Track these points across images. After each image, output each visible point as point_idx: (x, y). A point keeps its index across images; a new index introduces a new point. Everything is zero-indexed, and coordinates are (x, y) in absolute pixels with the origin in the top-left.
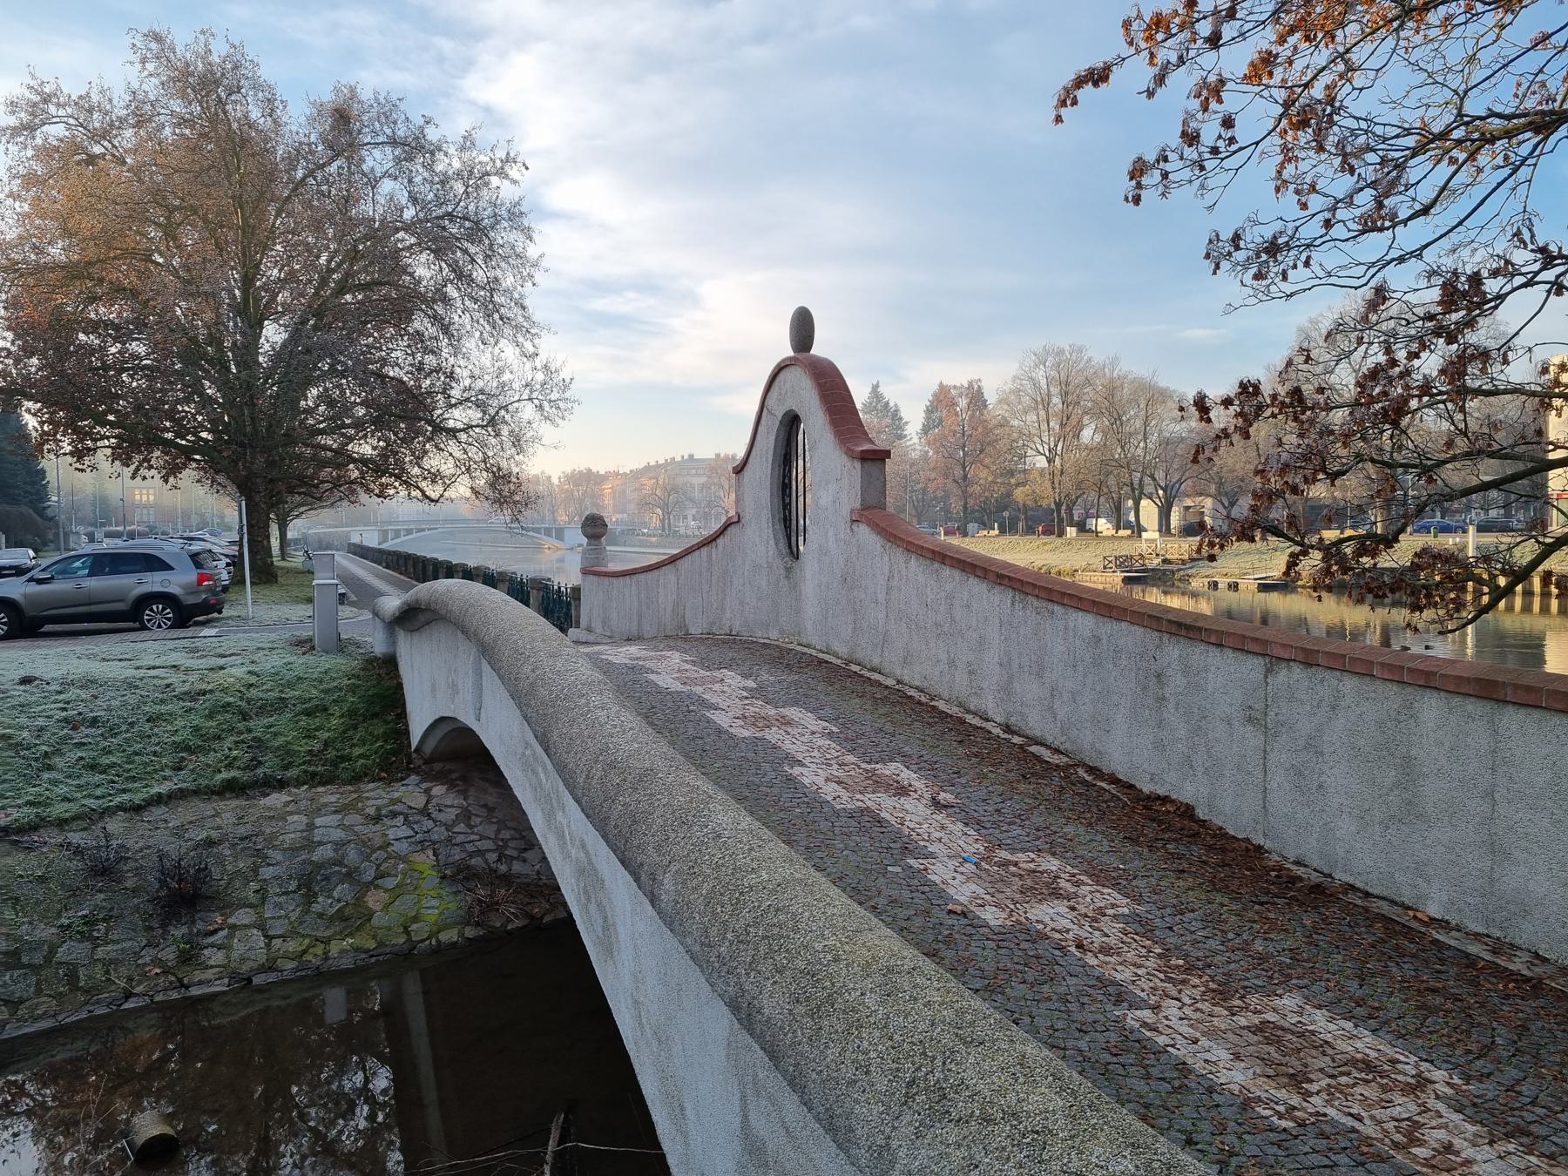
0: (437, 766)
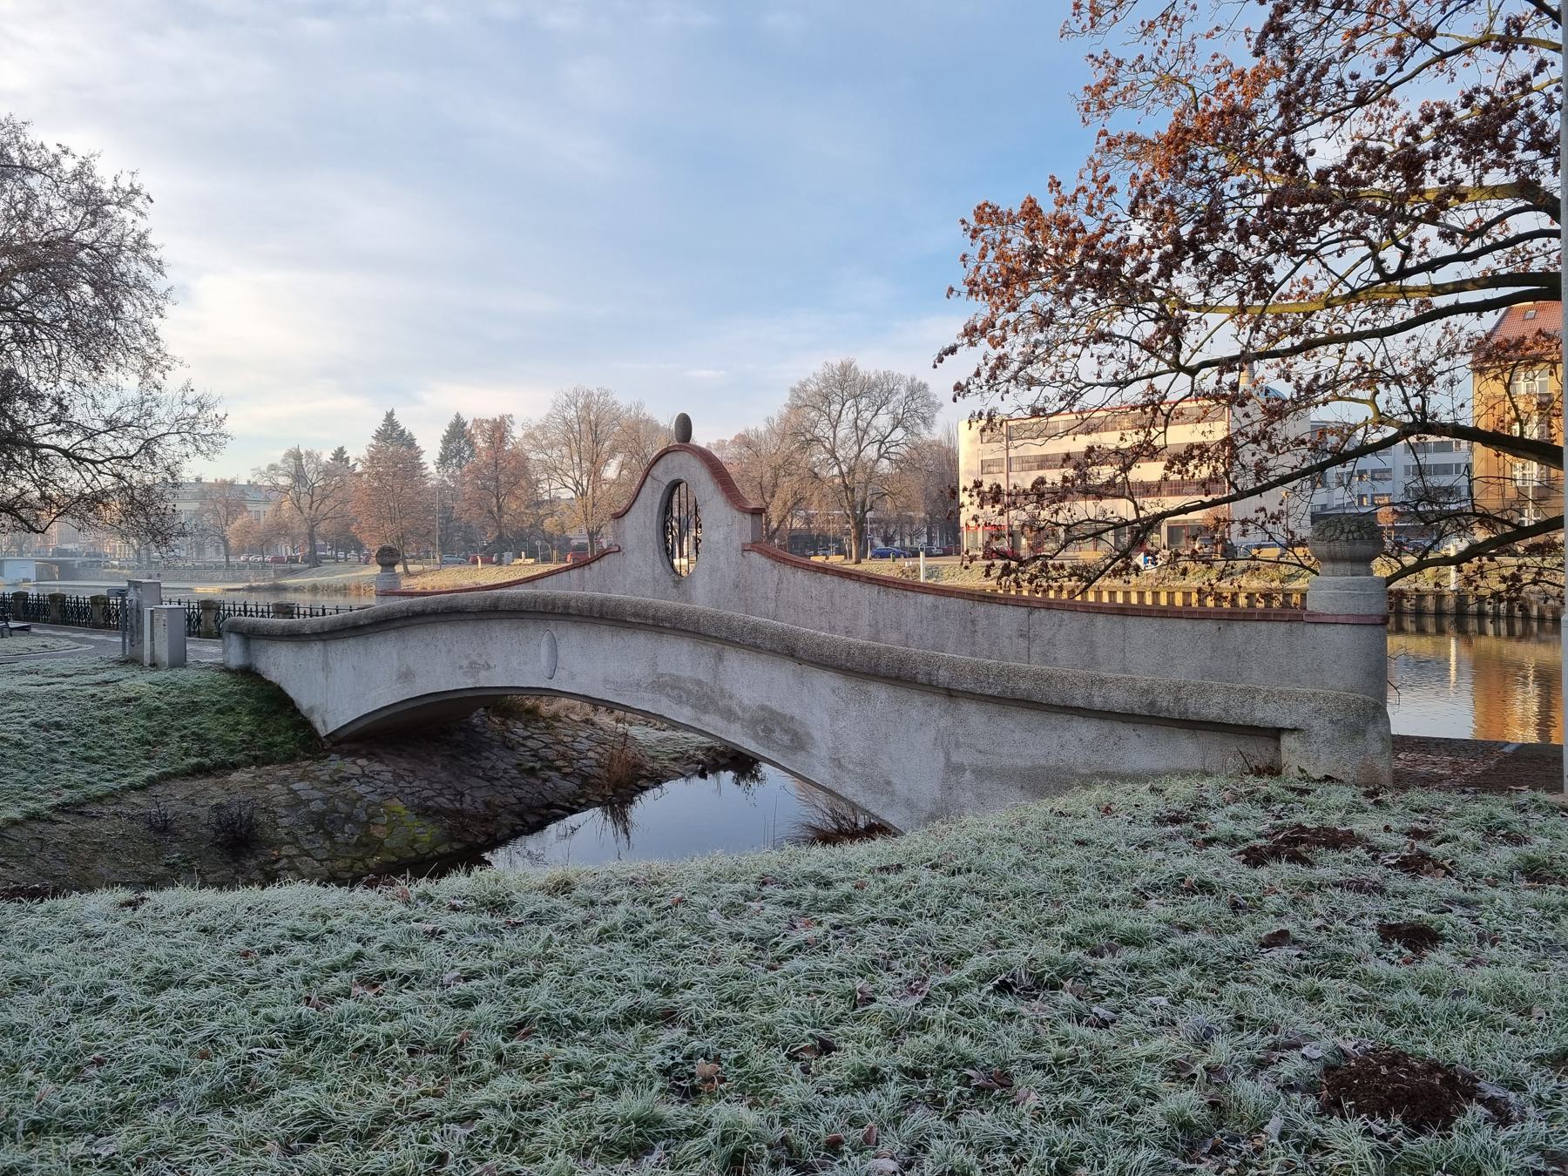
0: (345, 747)
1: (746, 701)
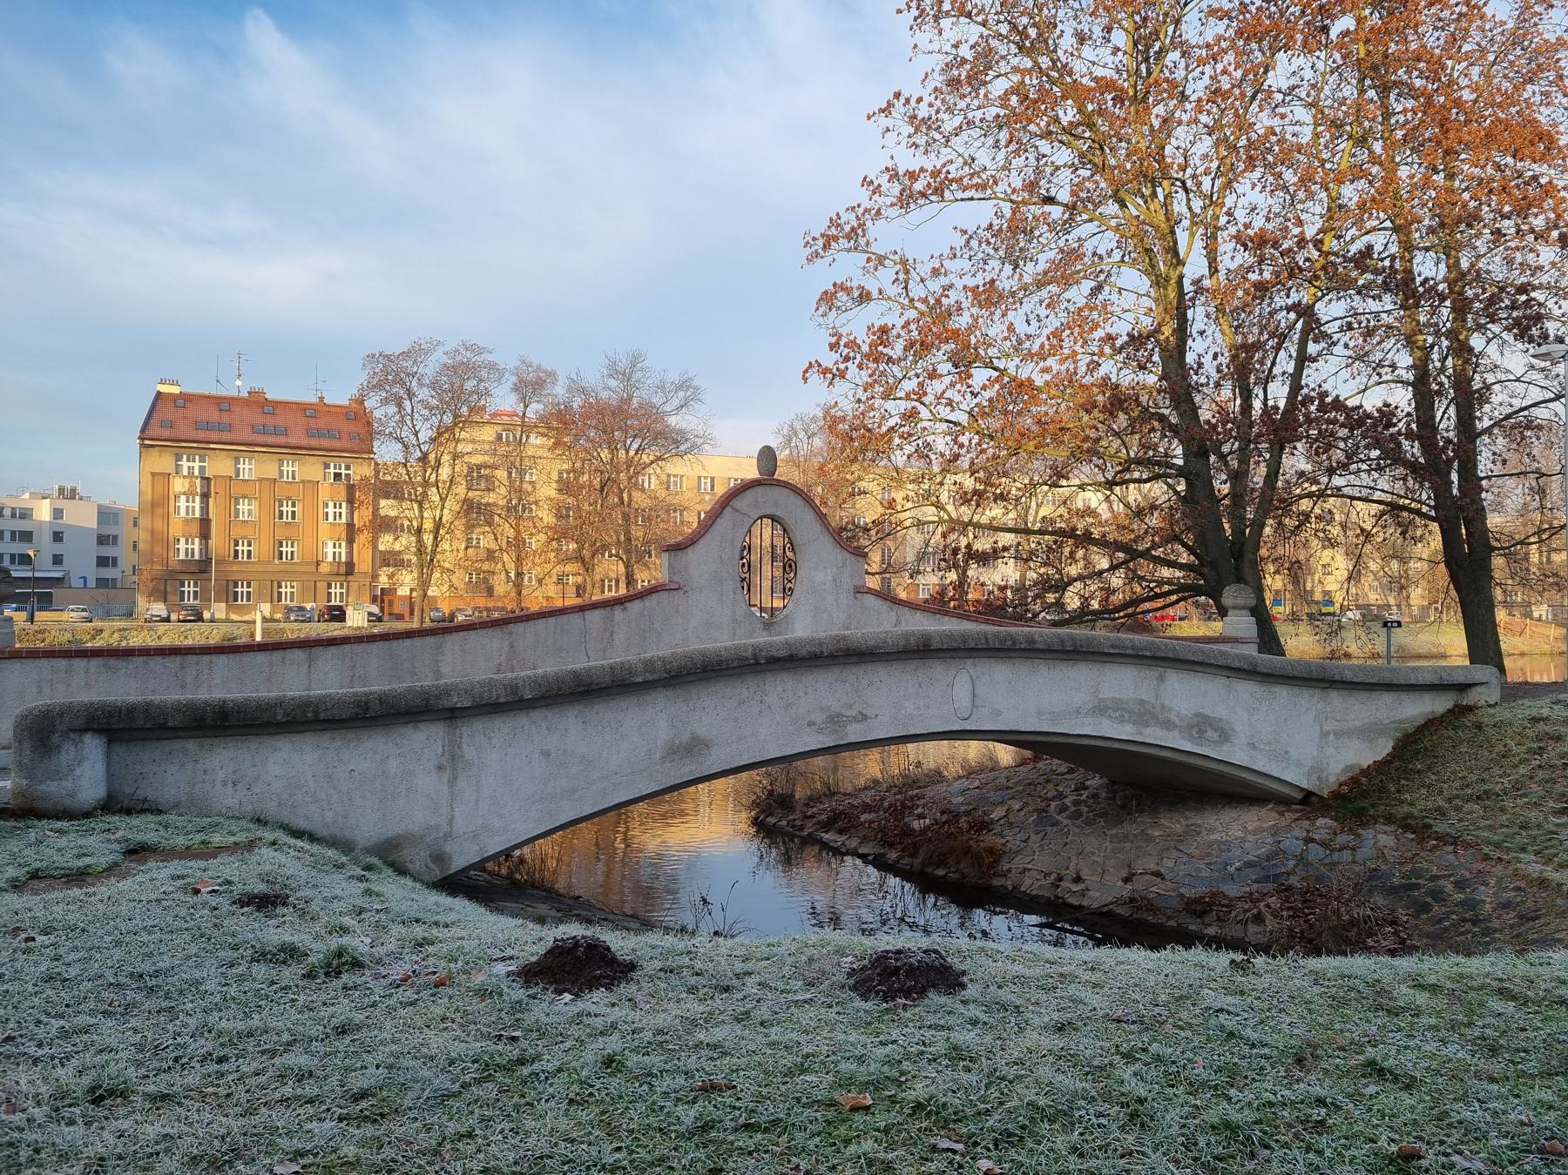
1: (1184, 712)
